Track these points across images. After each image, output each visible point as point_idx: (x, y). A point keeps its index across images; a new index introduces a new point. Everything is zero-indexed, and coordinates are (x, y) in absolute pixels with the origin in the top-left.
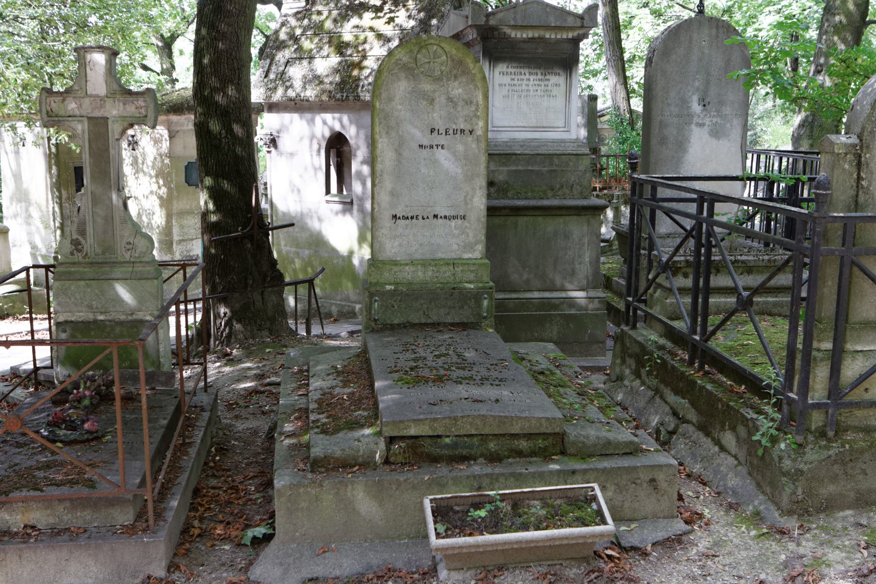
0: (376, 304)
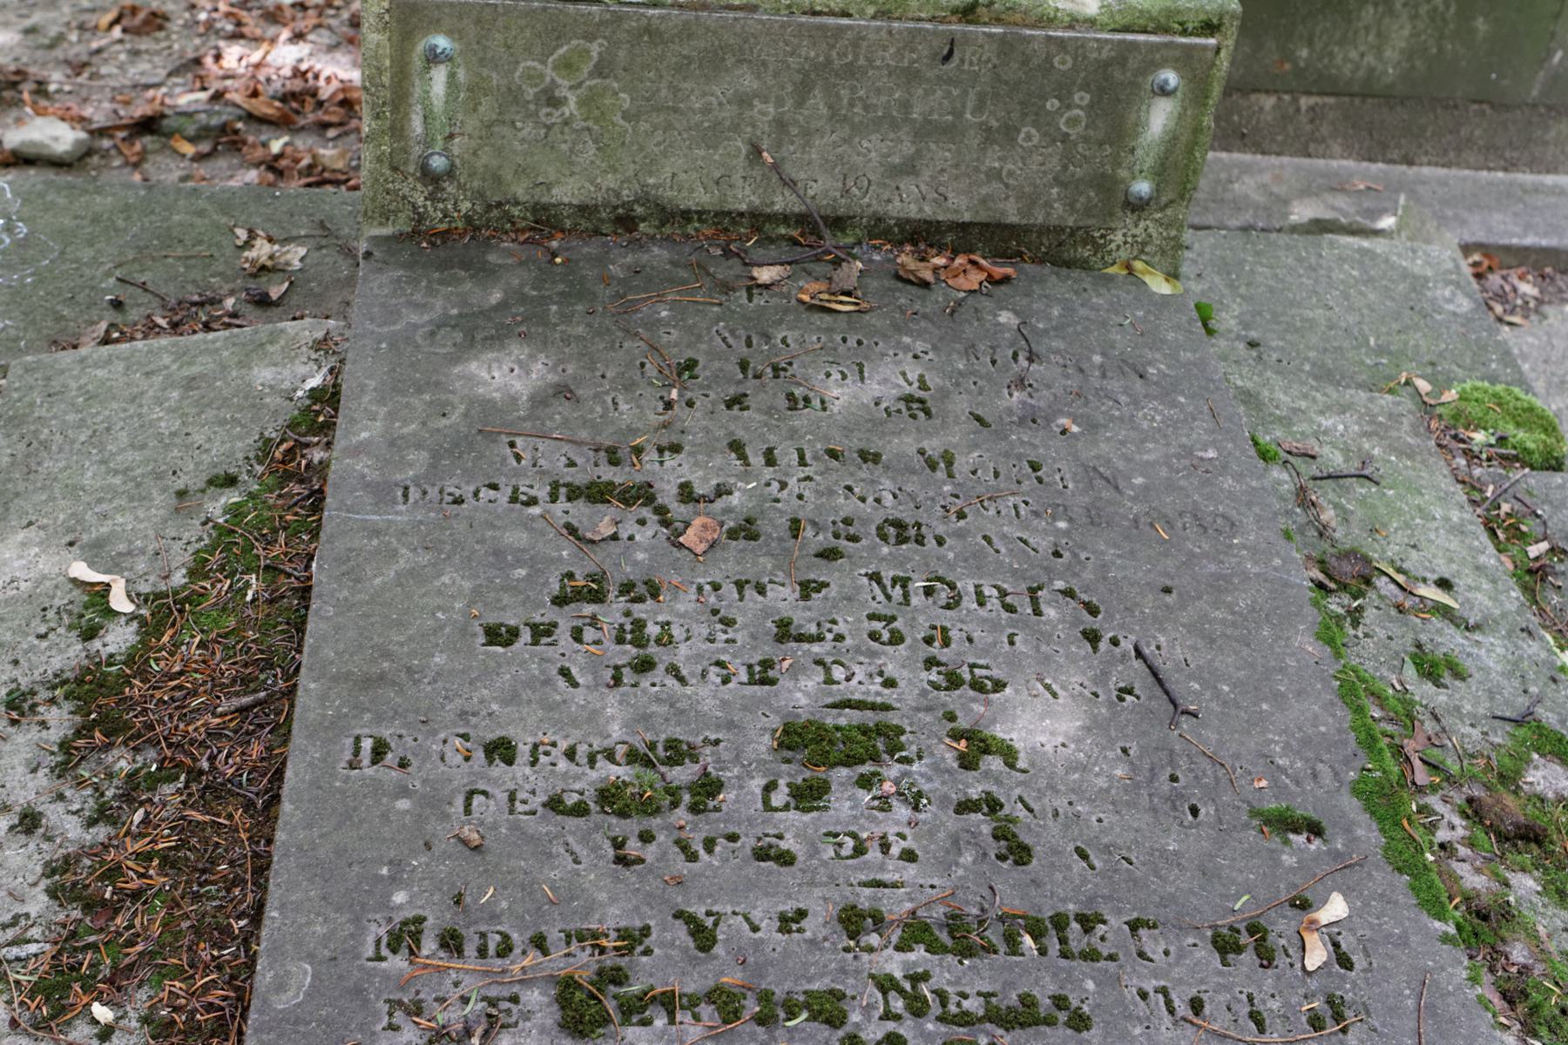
0: (439, 75)
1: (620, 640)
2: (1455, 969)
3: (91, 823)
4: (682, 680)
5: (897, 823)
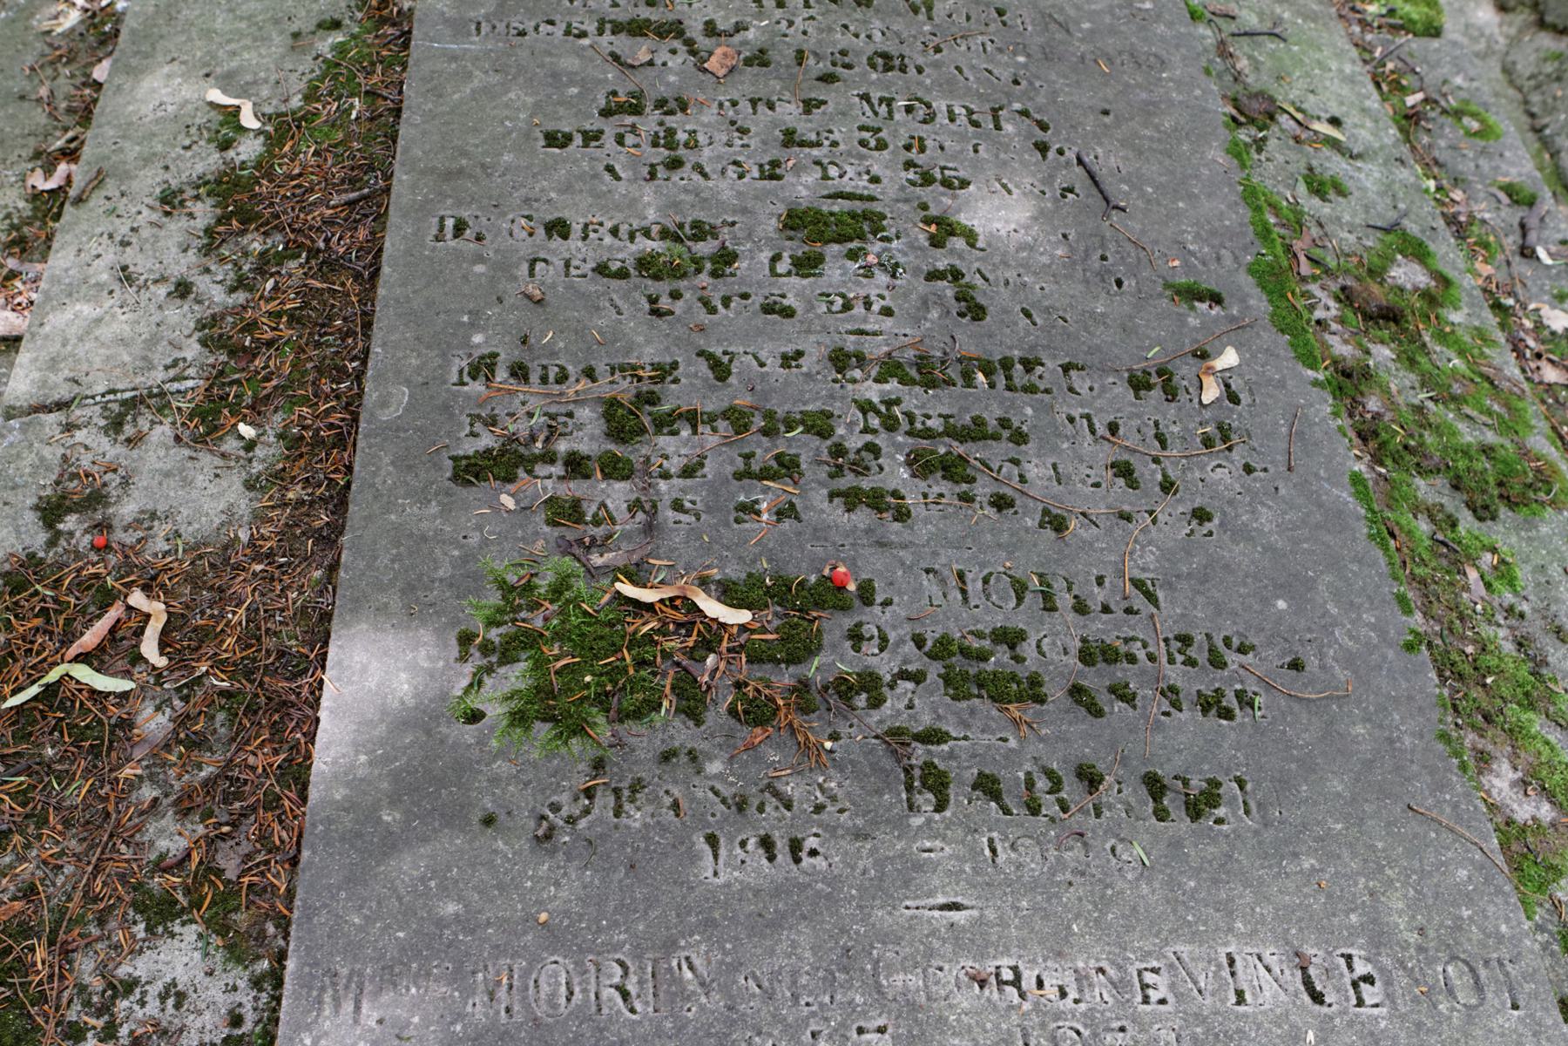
1: (655, 144)
2: (1324, 405)
3: (232, 290)
4: (705, 176)
5: (878, 287)
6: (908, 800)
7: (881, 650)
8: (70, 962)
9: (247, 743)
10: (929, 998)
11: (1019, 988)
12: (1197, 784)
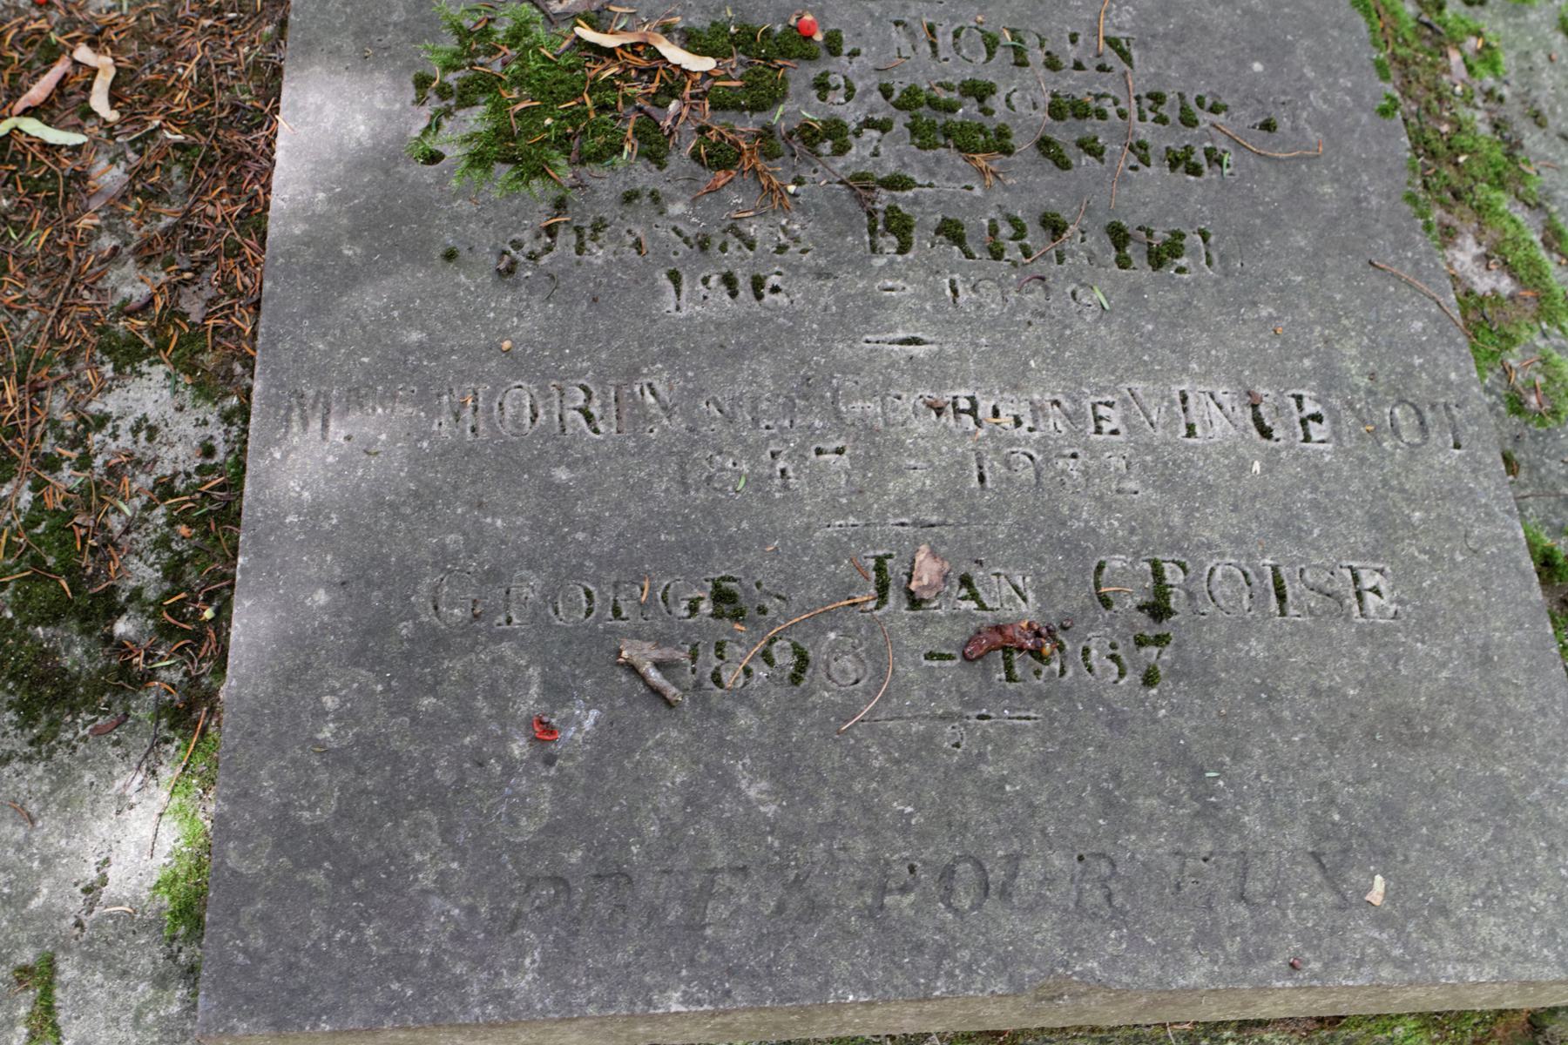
6: (871, 242)
7: (848, 99)
8: (41, 399)
9: (206, 192)
10: (887, 424)
11: (975, 417)
12: (1160, 235)
